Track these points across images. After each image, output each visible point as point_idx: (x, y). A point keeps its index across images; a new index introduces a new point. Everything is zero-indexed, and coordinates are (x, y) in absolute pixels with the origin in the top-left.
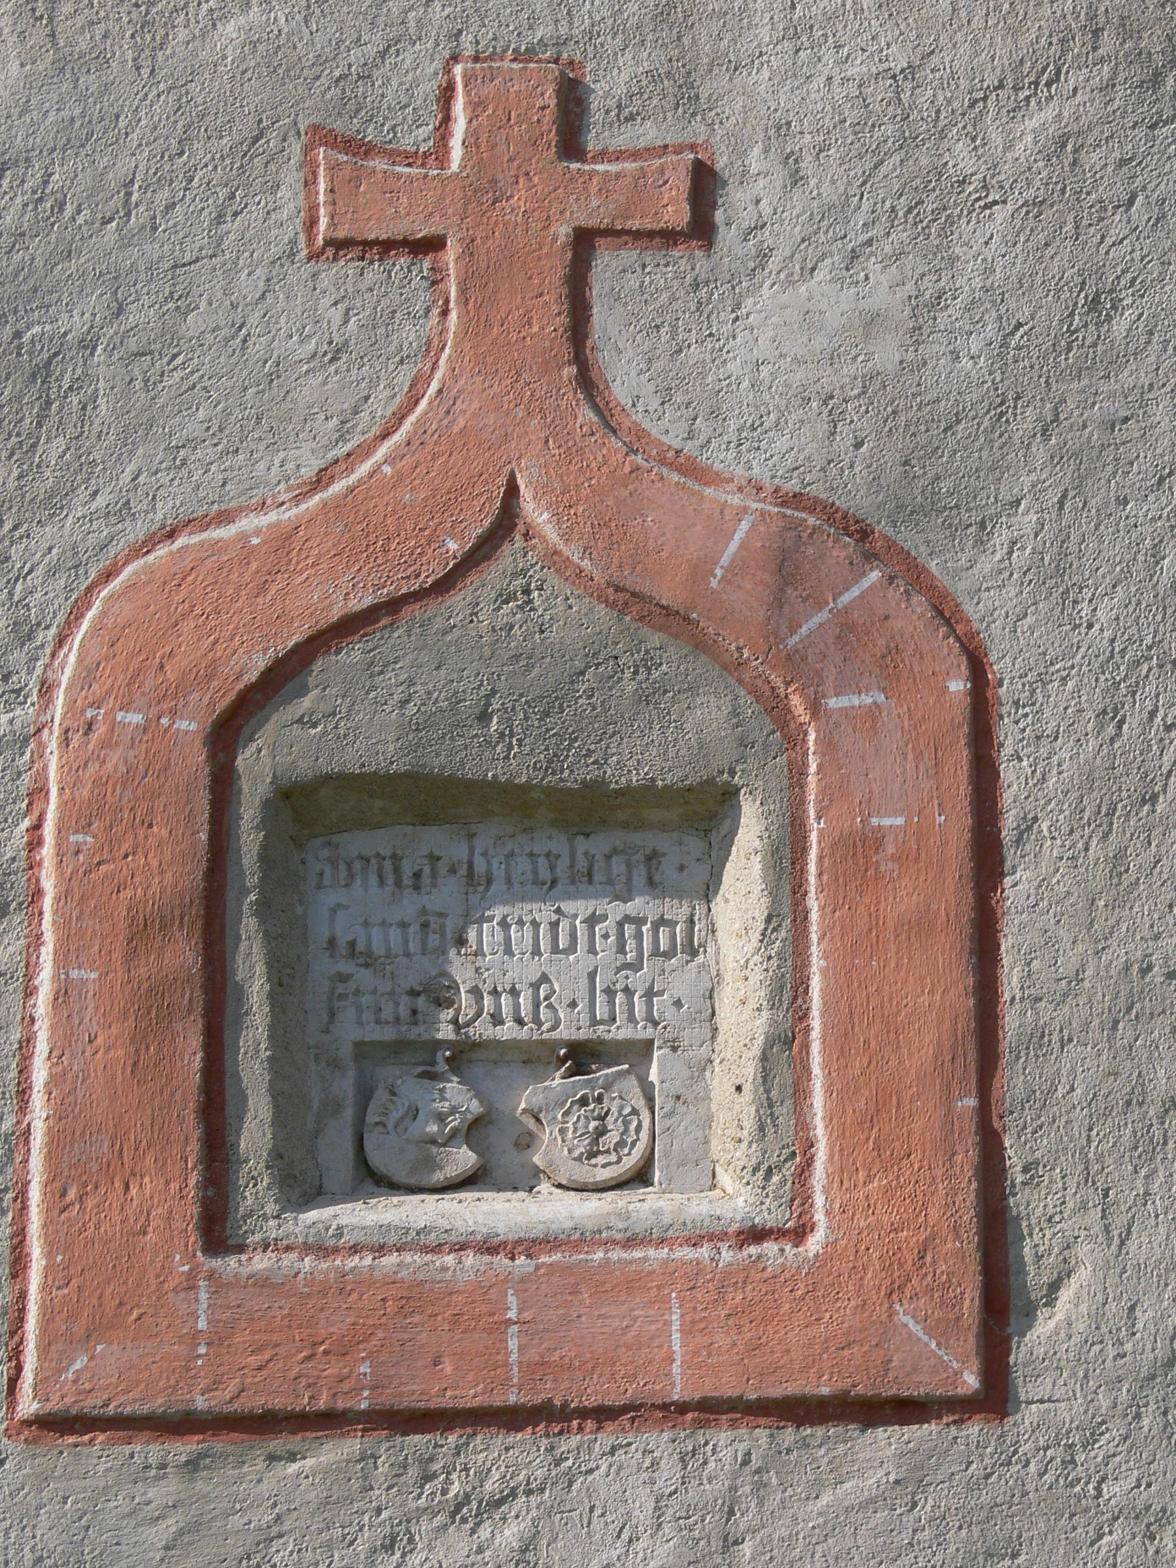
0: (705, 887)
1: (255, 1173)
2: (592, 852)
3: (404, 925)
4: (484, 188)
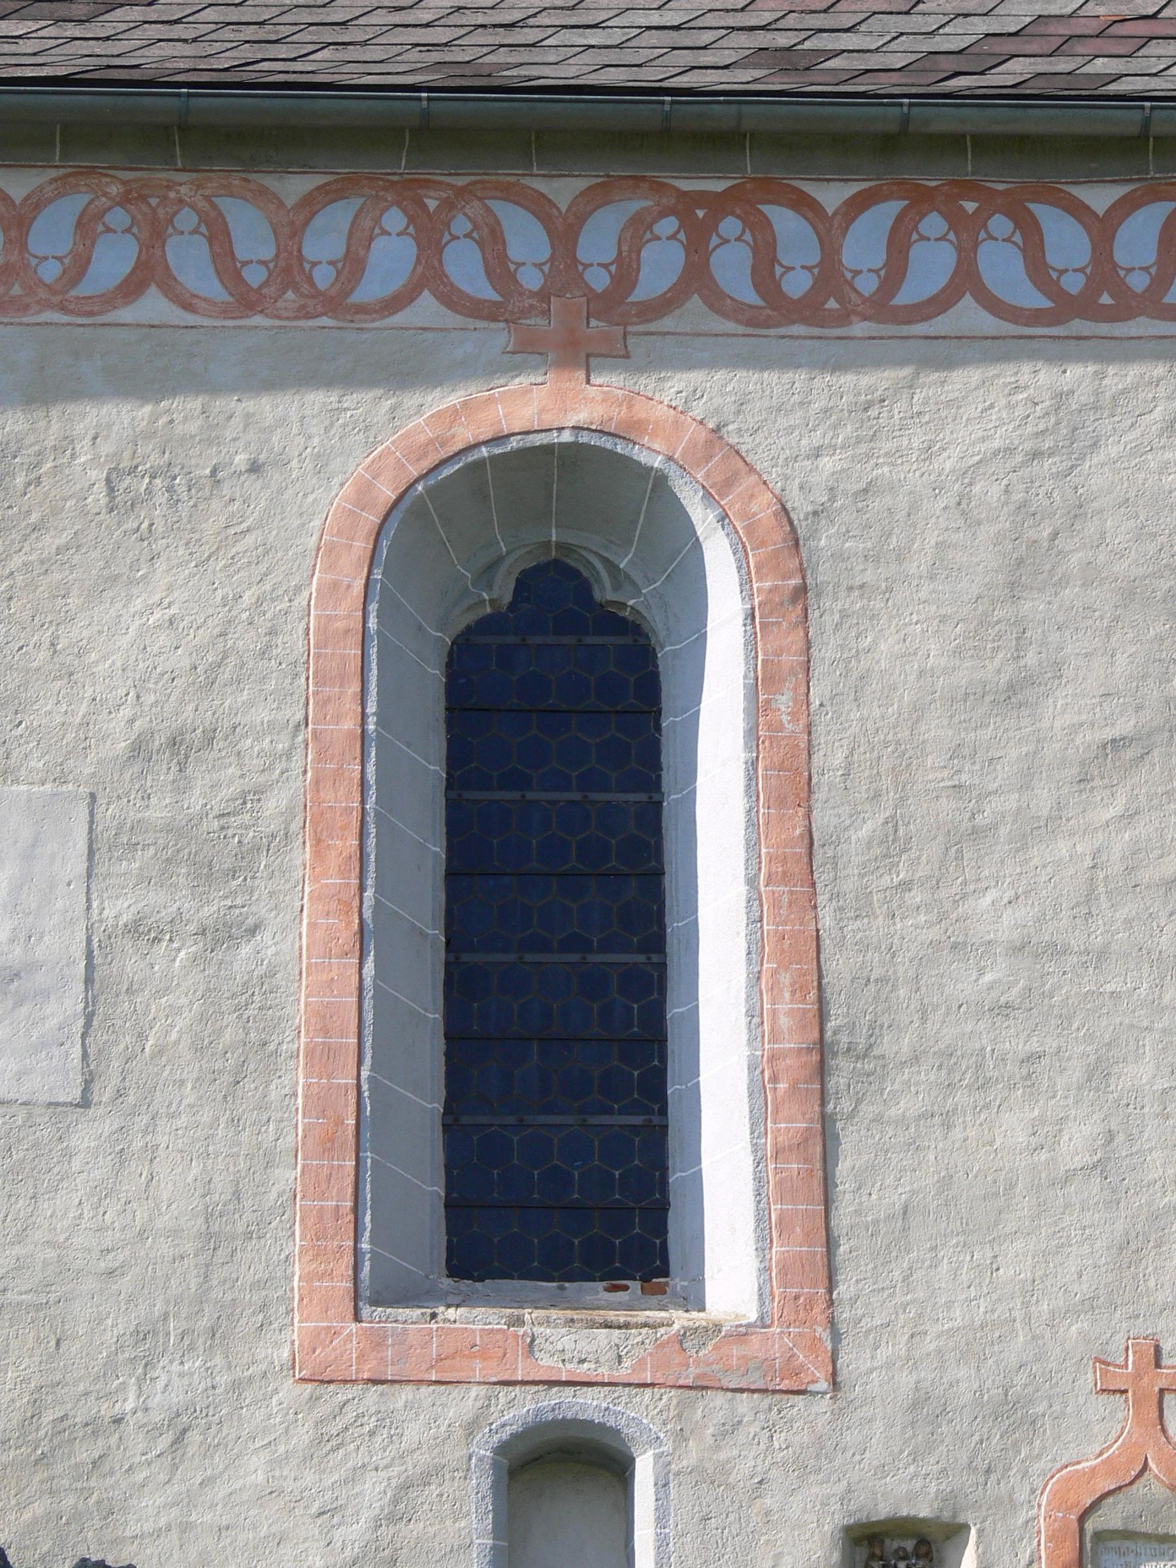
4: (1137, 1376)
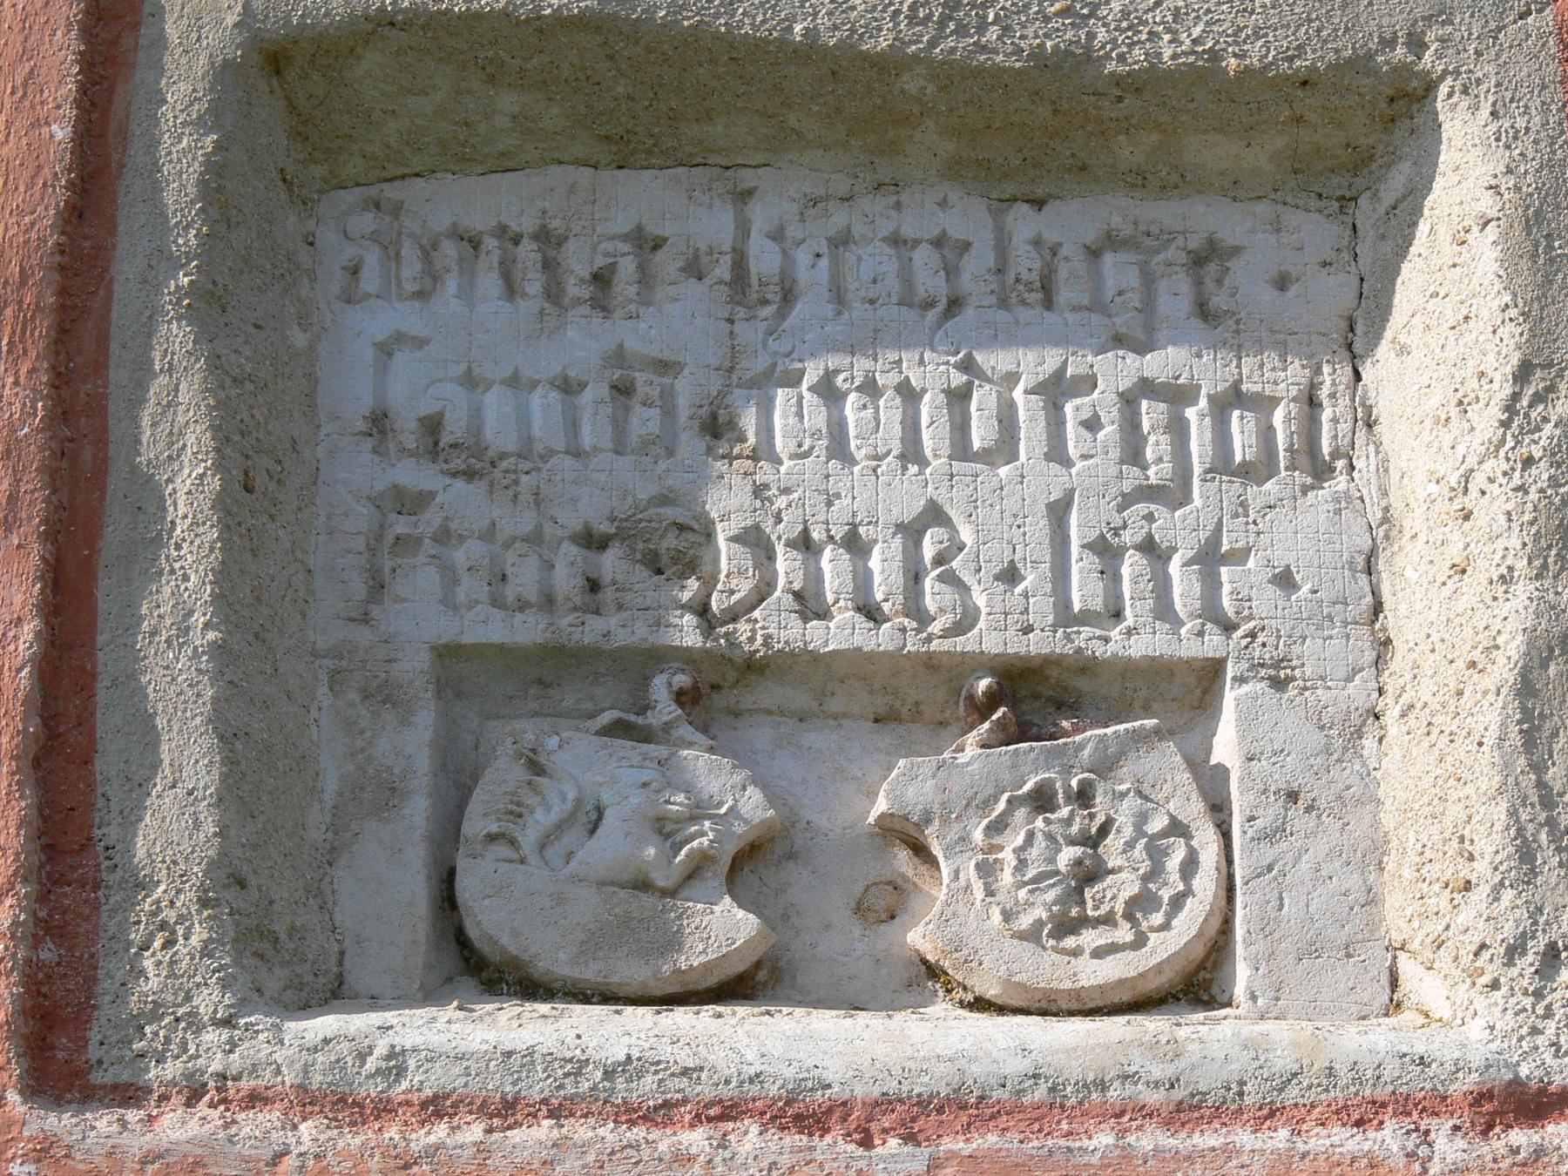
0: (1344, 325)
1: (170, 915)
2: (1051, 237)
3: (568, 387)
